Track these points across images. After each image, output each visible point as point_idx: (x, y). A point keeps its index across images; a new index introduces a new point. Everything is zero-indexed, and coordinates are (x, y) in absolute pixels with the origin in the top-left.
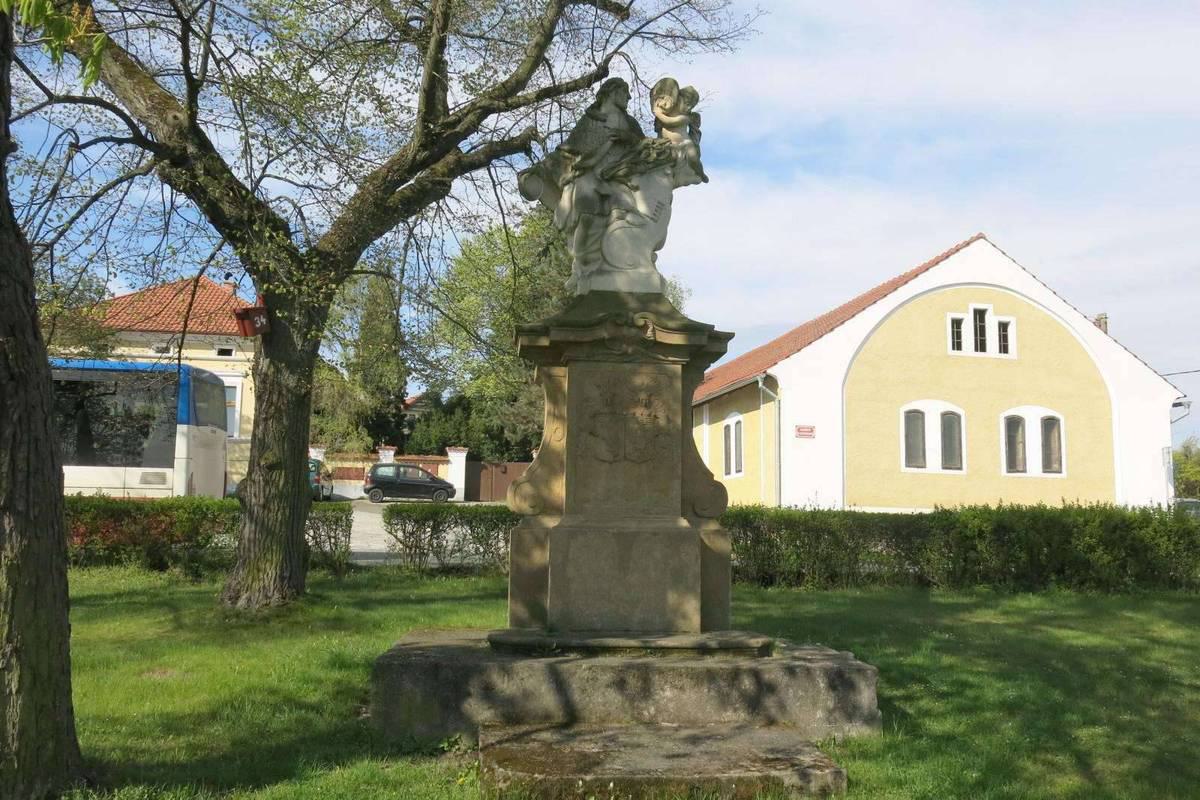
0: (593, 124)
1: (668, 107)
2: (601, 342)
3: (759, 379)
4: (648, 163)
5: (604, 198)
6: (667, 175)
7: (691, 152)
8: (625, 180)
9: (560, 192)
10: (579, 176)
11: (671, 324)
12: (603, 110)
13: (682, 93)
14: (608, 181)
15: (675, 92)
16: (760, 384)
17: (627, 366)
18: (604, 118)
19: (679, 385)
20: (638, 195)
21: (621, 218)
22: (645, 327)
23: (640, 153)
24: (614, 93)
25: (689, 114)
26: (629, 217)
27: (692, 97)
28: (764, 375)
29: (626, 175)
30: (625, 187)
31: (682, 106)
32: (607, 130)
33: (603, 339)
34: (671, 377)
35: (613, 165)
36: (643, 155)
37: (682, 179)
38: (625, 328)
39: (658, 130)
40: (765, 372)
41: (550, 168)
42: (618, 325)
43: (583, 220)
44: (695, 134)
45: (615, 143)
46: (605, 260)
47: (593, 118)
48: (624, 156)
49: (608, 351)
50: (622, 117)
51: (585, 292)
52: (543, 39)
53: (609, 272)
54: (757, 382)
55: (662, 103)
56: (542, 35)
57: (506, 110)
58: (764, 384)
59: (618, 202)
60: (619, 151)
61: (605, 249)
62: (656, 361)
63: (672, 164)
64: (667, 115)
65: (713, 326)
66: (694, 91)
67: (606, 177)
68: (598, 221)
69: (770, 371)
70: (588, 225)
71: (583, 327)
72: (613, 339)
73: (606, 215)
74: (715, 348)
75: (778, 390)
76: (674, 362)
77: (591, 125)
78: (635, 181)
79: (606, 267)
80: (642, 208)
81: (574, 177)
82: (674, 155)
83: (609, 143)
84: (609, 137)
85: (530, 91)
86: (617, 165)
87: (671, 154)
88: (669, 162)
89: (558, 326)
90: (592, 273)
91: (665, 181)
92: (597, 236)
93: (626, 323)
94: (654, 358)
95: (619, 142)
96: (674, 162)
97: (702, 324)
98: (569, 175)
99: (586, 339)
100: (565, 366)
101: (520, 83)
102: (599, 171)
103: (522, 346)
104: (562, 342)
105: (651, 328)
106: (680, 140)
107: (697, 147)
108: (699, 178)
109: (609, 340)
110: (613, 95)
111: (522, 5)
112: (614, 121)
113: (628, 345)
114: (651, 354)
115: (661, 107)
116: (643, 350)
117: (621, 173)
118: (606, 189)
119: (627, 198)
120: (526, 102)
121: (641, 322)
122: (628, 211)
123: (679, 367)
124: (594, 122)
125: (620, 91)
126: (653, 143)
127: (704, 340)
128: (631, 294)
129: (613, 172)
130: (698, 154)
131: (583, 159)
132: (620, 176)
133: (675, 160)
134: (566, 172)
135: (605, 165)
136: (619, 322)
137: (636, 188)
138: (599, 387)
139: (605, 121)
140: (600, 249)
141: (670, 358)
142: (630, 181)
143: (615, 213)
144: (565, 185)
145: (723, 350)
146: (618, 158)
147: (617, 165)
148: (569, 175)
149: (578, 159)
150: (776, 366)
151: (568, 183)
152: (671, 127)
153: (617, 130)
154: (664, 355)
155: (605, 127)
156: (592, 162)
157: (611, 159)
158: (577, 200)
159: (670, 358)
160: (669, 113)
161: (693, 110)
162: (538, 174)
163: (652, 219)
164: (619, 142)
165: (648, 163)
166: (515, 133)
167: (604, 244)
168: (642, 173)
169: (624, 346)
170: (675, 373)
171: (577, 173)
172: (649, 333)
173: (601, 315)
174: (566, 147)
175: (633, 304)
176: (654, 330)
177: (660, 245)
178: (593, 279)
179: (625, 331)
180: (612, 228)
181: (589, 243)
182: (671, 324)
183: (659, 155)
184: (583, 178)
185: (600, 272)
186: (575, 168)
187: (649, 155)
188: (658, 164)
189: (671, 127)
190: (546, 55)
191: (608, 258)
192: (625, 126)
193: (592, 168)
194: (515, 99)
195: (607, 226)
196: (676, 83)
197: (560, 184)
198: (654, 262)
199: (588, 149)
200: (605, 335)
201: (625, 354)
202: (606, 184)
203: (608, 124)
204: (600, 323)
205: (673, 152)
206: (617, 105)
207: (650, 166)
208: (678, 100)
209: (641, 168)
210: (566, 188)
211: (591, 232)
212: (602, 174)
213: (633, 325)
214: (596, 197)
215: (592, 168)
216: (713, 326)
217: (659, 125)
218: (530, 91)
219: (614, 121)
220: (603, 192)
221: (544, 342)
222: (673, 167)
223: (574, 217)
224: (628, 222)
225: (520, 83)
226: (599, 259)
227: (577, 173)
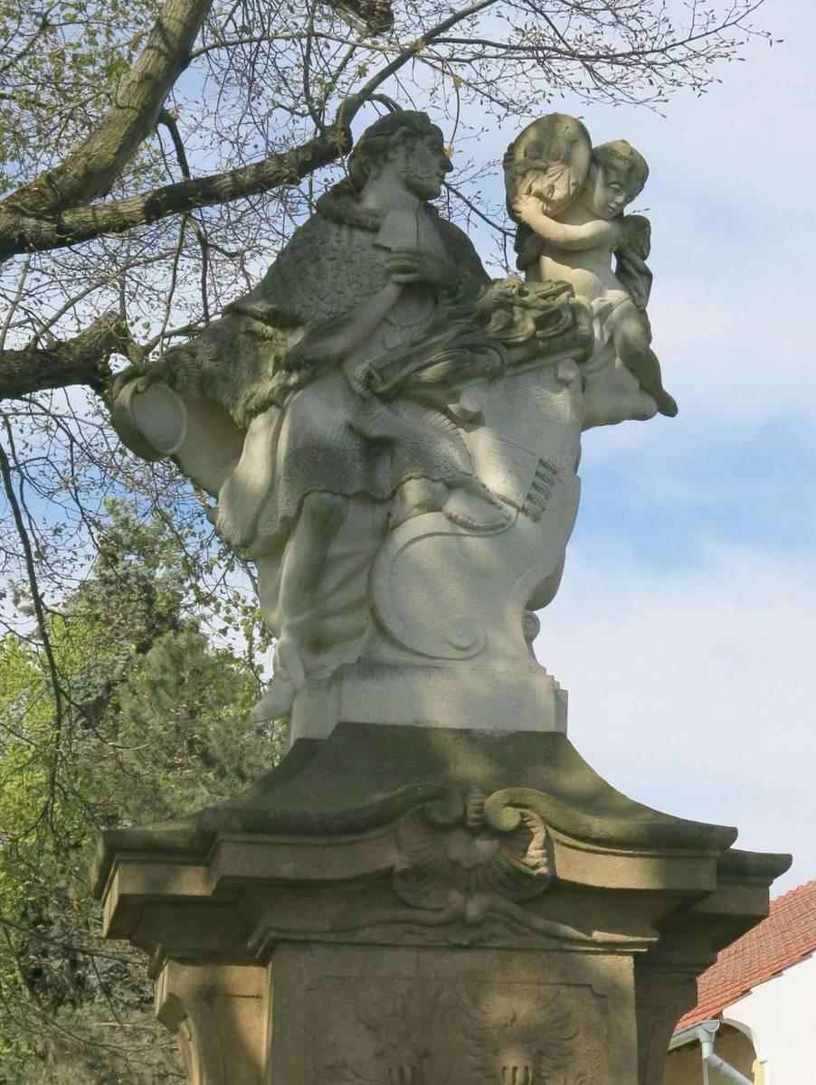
0: (339, 238)
1: (559, 194)
2: (381, 883)
3: (703, 1036)
4: (510, 346)
5: (376, 447)
6: (565, 383)
7: (631, 328)
8: (438, 395)
9: (236, 436)
10: (298, 387)
11: (601, 825)
12: (371, 201)
13: (601, 159)
14: (386, 398)
15: (581, 156)
16: (706, 1050)
17: (465, 960)
18: (370, 221)
19: (628, 1021)
20: (481, 442)
21: (433, 506)
22: (520, 835)
23: (484, 318)
24: (402, 150)
25: (619, 217)
26: (455, 505)
27: (632, 174)
28: (715, 1026)
29: (445, 382)
30: (438, 419)
31: (599, 193)
32: (382, 256)
33: (389, 873)
34: (604, 995)
35: (403, 353)
36: (494, 326)
37: (602, 405)
38: (459, 834)
39: (529, 264)
40: (718, 1016)
41: (208, 365)
42: (436, 829)
43: (313, 513)
44: (634, 276)
45: (407, 289)
46: (382, 630)
47: (339, 220)
48: (435, 329)
49: (404, 913)
50: (427, 223)
51: (324, 729)
52: (162, 63)
53: (394, 668)
54: (696, 1044)
55: (540, 185)
56: (161, 52)
57: (61, 243)
58: (716, 1049)
59: (425, 462)
60: (418, 318)
61: (382, 600)
62: (554, 943)
63: (579, 352)
64: (555, 218)
65: (732, 833)
66: (633, 152)
67: (382, 388)
68: (360, 518)
69: (733, 1013)
70: (327, 527)
71: (327, 832)
72: (419, 873)
73: (384, 500)
74: (731, 903)
75: (756, 1067)
76: (611, 948)
77: (333, 242)
78: (469, 400)
79: (386, 653)
80: (496, 480)
81: (285, 390)
82: (583, 328)
83: (390, 292)
84: (388, 273)
85: (130, 193)
86: (416, 352)
87: (575, 324)
88: (566, 348)
89: (247, 830)
90: (338, 676)
91: (561, 402)
92: (350, 565)
93: (461, 823)
94: (551, 935)
95: (419, 289)
96: (584, 349)
97: (692, 822)
98: (268, 386)
99: (331, 874)
100: (263, 962)
101: (98, 178)
102: (358, 369)
103: (122, 898)
104: (258, 882)
105: (539, 837)
106: (597, 291)
107: (641, 312)
108: (650, 403)
109: (404, 875)
110: (399, 159)
111: (91, 10)
112: (403, 230)
113: (468, 892)
114: (540, 923)
115: (539, 196)
116: (516, 910)
117: (428, 375)
118: (381, 422)
119: (447, 449)
120: (121, 225)
121: (510, 819)
122: (451, 486)
123: (628, 961)
124: (345, 234)
125: (421, 146)
126: (522, 293)
127: (705, 878)
128: (465, 734)
129: (406, 371)
130: (648, 336)
131: (313, 337)
132: (427, 385)
133: (588, 341)
134: (256, 373)
135: (377, 354)
136: (439, 818)
137: (473, 421)
138: (372, 1027)
139: (375, 230)
140: (367, 602)
141: (598, 935)
142: (455, 397)
143: (414, 491)
144: (252, 414)
145: (757, 911)
146: (417, 332)
147: (416, 352)
148: (268, 386)
149: (295, 339)
150: (747, 1000)
151: (263, 407)
152: (568, 252)
153: (416, 254)
154: (576, 927)
155: (377, 246)
156: (337, 344)
157: (396, 339)
158: (295, 456)
159: (598, 935)
160: (561, 212)
161: (628, 210)
162: (172, 382)
163: (523, 510)
164: (419, 289)
165: (510, 346)
166: (66, 330)
167: (381, 582)
168: (493, 376)
169: (455, 896)
170: (614, 986)
171: (293, 379)
172: (535, 853)
173: (379, 797)
174: (260, 307)
175: (471, 767)
176: (548, 845)
177: (543, 594)
178: (347, 686)
179: (458, 848)
180: (402, 536)
181: (330, 582)
182: (601, 825)
183: (540, 323)
184: (311, 388)
185: (369, 667)
186: (291, 363)
187: (511, 325)
188: (536, 354)
189: (568, 252)
190: (169, 106)
191: (393, 625)
192: (431, 242)
193: (339, 362)
194: (84, 214)
195: (386, 530)
196: (583, 131)
197: (238, 414)
198: (529, 639)
199: (322, 309)
200: (395, 859)
201: (459, 920)
202: (380, 410)
203: (381, 239)
204: (379, 820)
205: (583, 319)
206: (410, 186)
207: (517, 354)
208: (589, 177)
209: (493, 358)
210: (259, 423)
211: (336, 549)
212: (369, 380)
213: (486, 828)
214: (352, 446)
215: (339, 362)
216: (732, 833)
217: (530, 246)
218: (130, 193)
219: (403, 230)
220: (376, 431)
221: (192, 884)
222: (582, 360)
223: (284, 504)
224: (451, 519)
225: (98, 178)
226: (360, 633)
227: (293, 379)
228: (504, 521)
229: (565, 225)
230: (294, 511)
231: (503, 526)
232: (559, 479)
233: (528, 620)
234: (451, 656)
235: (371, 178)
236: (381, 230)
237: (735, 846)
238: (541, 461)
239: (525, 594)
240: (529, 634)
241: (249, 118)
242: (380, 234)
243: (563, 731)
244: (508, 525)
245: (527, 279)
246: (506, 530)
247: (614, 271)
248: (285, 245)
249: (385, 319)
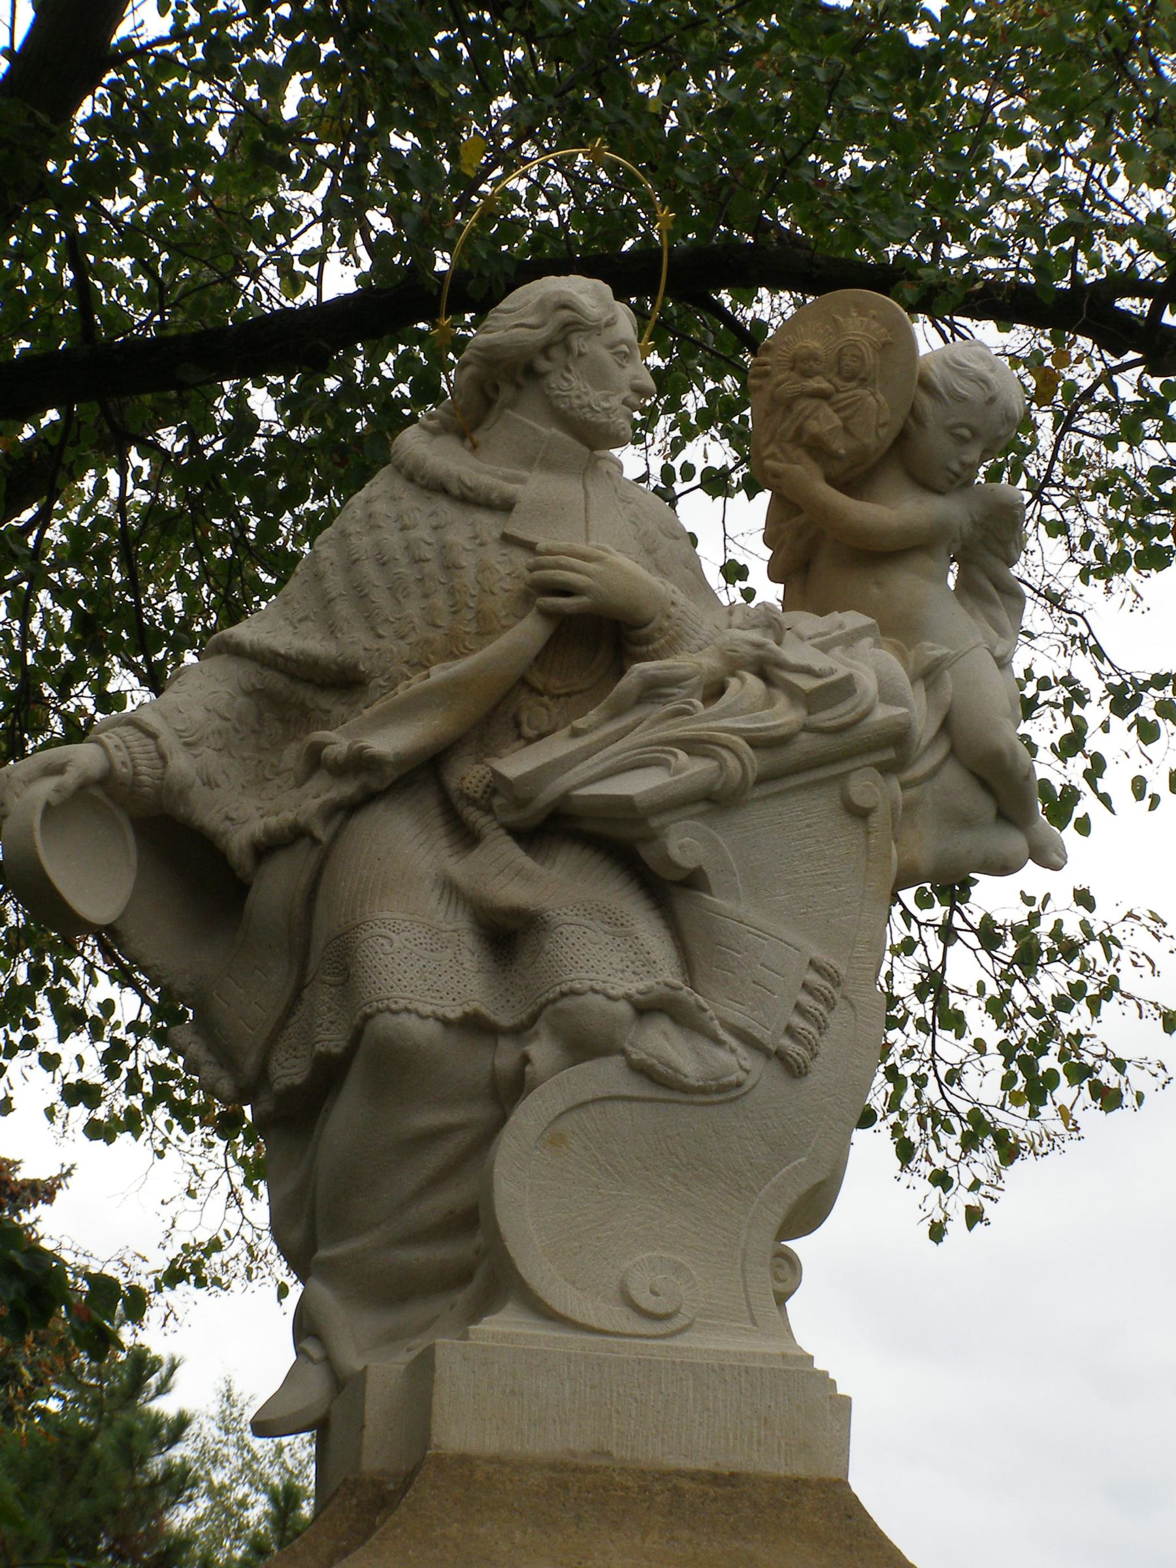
65: (15, 1164)
155: (508, 540)
216: (15, 1164)
228: (741, 1075)
229: (865, 503)
230: (344, 1043)
231: (739, 1085)
232: (844, 997)
233: (781, 1261)
234: (629, 1331)
235: (497, 405)
236: (515, 509)
237: (19, 1176)
238: (811, 963)
239: (776, 1215)
240: (780, 1287)
241: (1102, 392)
242: (513, 514)
243: (832, 1474)
244: (750, 1082)
245: (787, 603)
246: (745, 1094)
247: (953, 588)
248: (88, 483)
249: (523, 682)
